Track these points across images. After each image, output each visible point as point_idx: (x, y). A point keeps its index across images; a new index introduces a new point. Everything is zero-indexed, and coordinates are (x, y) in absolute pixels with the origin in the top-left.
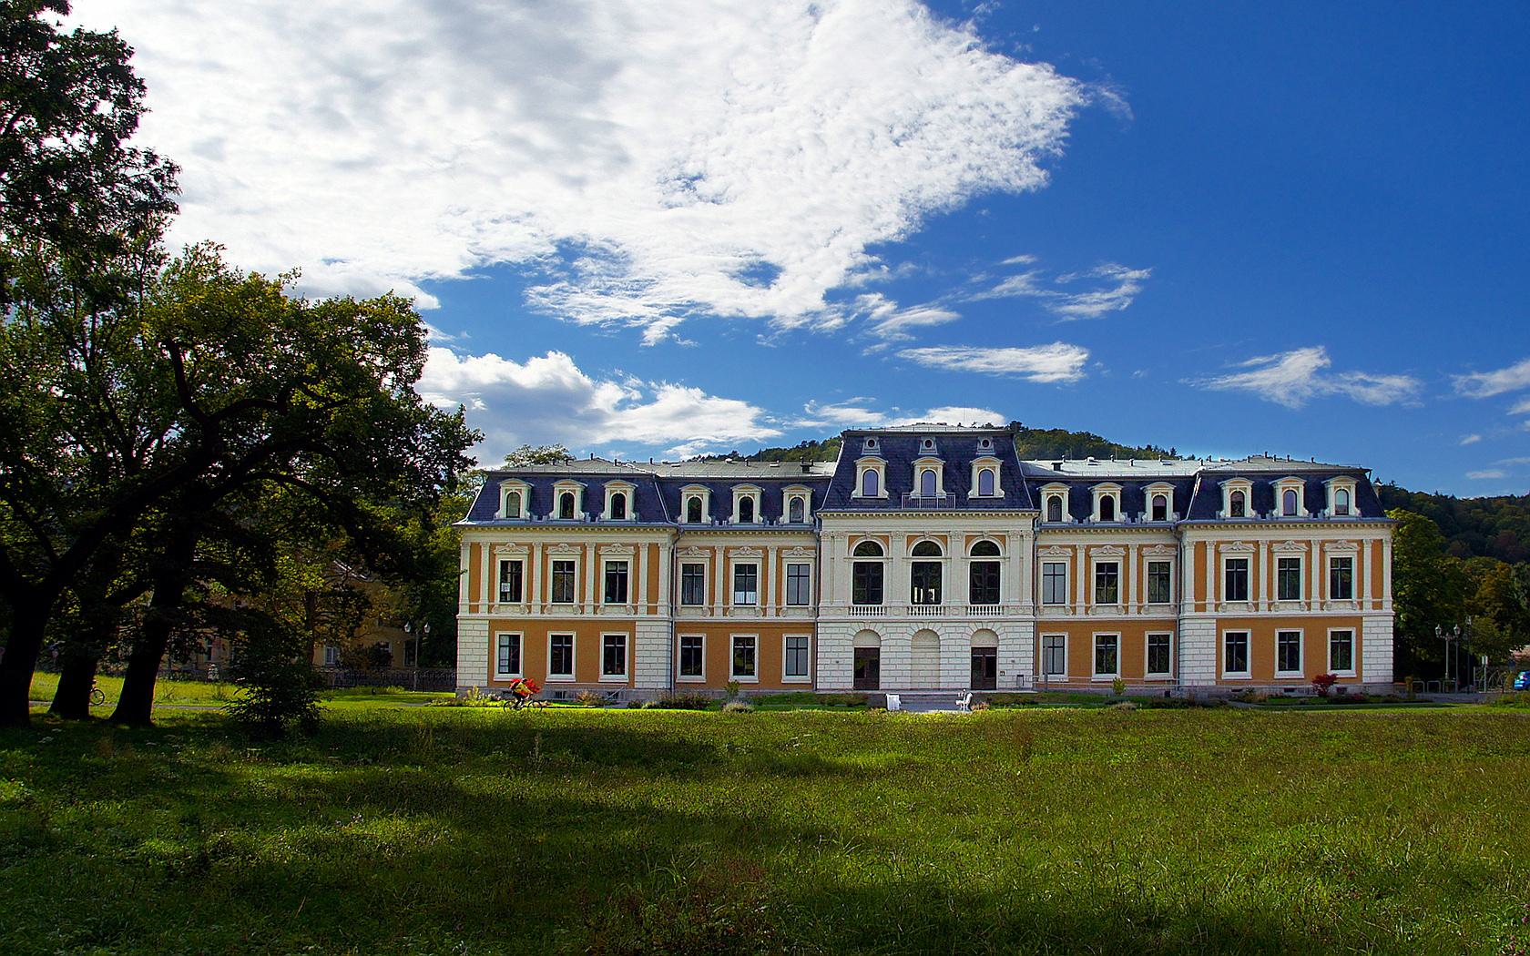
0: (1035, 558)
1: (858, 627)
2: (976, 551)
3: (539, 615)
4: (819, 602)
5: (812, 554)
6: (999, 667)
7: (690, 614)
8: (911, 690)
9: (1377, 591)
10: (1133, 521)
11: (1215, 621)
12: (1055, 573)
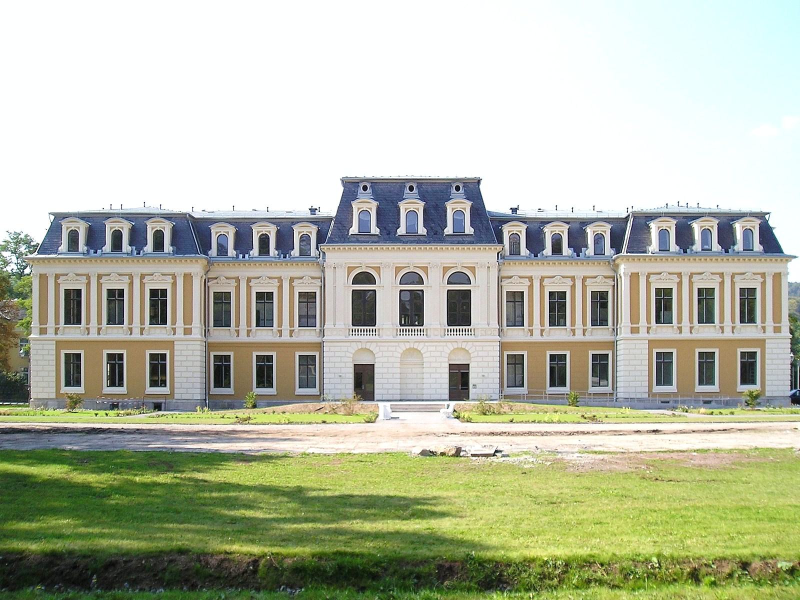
0: (500, 289)
1: (451, 347)
2: (356, 281)
3: (96, 336)
4: (324, 324)
5: (318, 283)
6: (472, 382)
7: (220, 335)
8: (401, 400)
9: (188, 319)
10: (578, 256)
11: (55, 342)
12: (516, 298)
